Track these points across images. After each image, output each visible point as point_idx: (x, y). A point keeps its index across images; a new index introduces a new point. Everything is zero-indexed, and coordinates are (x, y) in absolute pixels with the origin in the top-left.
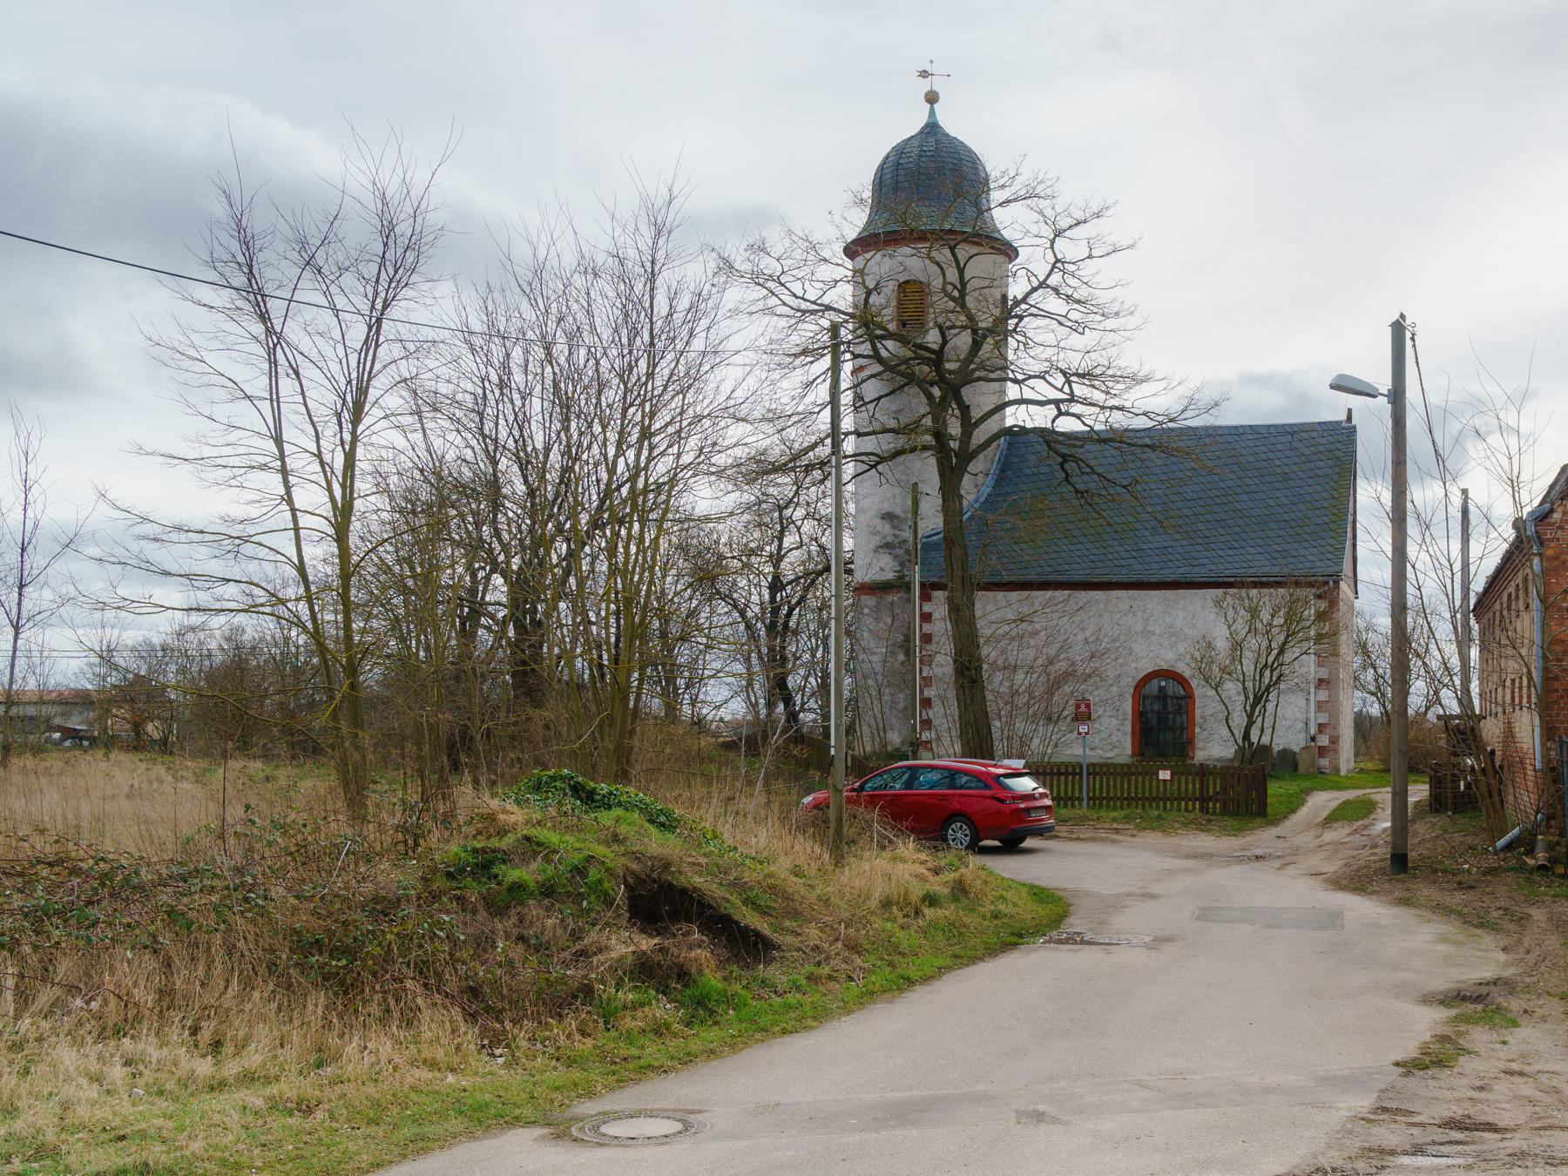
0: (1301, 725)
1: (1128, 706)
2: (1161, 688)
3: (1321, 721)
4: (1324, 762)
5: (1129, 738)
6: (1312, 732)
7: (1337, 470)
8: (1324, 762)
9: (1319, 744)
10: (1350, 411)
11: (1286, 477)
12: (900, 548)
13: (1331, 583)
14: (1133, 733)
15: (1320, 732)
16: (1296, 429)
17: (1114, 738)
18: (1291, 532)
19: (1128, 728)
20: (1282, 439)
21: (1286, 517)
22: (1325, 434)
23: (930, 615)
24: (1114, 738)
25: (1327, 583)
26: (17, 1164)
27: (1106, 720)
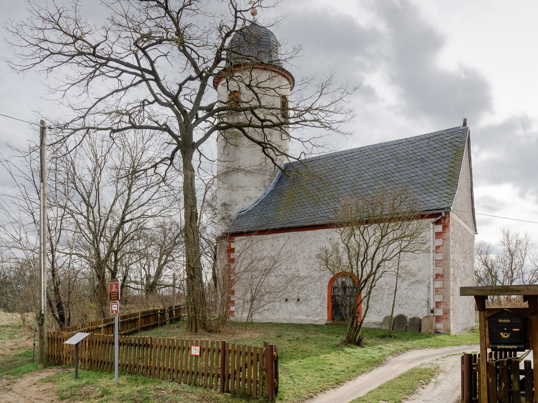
0: (424, 303)
1: (325, 293)
2: (343, 283)
3: (438, 300)
4: (439, 326)
5: (326, 310)
6: (432, 307)
7: (454, 152)
8: (439, 326)
9: (436, 314)
10: (465, 120)
11: (423, 161)
12: (228, 219)
13: (443, 214)
14: (328, 308)
15: (437, 307)
16: (431, 136)
17: (319, 310)
18: (422, 188)
19: (326, 305)
20: (424, 142)
21: (420, 181)
22: (449, 135)
23: (234, 249)
24: (319, 310)
25: (441, 214)
26: (195, 401)
27: (314, 301)
